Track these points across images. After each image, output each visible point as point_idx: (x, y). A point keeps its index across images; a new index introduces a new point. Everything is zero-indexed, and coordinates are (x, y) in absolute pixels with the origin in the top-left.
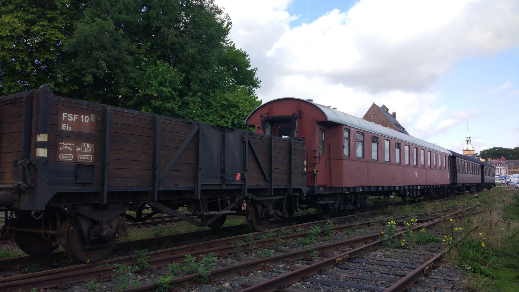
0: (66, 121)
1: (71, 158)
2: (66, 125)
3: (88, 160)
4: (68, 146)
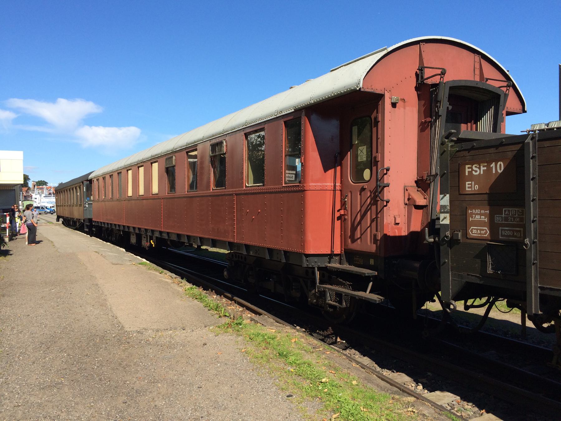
0: (471, 177)
1: (485, 233)
2: (470, 182)
3: (516, 237)
4: (481, 215)
